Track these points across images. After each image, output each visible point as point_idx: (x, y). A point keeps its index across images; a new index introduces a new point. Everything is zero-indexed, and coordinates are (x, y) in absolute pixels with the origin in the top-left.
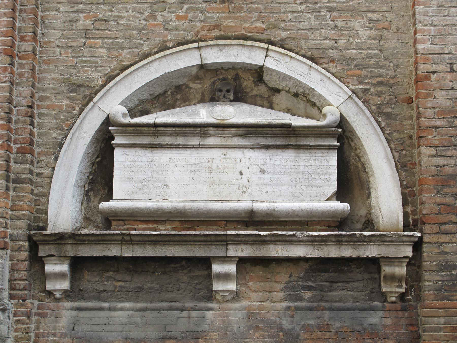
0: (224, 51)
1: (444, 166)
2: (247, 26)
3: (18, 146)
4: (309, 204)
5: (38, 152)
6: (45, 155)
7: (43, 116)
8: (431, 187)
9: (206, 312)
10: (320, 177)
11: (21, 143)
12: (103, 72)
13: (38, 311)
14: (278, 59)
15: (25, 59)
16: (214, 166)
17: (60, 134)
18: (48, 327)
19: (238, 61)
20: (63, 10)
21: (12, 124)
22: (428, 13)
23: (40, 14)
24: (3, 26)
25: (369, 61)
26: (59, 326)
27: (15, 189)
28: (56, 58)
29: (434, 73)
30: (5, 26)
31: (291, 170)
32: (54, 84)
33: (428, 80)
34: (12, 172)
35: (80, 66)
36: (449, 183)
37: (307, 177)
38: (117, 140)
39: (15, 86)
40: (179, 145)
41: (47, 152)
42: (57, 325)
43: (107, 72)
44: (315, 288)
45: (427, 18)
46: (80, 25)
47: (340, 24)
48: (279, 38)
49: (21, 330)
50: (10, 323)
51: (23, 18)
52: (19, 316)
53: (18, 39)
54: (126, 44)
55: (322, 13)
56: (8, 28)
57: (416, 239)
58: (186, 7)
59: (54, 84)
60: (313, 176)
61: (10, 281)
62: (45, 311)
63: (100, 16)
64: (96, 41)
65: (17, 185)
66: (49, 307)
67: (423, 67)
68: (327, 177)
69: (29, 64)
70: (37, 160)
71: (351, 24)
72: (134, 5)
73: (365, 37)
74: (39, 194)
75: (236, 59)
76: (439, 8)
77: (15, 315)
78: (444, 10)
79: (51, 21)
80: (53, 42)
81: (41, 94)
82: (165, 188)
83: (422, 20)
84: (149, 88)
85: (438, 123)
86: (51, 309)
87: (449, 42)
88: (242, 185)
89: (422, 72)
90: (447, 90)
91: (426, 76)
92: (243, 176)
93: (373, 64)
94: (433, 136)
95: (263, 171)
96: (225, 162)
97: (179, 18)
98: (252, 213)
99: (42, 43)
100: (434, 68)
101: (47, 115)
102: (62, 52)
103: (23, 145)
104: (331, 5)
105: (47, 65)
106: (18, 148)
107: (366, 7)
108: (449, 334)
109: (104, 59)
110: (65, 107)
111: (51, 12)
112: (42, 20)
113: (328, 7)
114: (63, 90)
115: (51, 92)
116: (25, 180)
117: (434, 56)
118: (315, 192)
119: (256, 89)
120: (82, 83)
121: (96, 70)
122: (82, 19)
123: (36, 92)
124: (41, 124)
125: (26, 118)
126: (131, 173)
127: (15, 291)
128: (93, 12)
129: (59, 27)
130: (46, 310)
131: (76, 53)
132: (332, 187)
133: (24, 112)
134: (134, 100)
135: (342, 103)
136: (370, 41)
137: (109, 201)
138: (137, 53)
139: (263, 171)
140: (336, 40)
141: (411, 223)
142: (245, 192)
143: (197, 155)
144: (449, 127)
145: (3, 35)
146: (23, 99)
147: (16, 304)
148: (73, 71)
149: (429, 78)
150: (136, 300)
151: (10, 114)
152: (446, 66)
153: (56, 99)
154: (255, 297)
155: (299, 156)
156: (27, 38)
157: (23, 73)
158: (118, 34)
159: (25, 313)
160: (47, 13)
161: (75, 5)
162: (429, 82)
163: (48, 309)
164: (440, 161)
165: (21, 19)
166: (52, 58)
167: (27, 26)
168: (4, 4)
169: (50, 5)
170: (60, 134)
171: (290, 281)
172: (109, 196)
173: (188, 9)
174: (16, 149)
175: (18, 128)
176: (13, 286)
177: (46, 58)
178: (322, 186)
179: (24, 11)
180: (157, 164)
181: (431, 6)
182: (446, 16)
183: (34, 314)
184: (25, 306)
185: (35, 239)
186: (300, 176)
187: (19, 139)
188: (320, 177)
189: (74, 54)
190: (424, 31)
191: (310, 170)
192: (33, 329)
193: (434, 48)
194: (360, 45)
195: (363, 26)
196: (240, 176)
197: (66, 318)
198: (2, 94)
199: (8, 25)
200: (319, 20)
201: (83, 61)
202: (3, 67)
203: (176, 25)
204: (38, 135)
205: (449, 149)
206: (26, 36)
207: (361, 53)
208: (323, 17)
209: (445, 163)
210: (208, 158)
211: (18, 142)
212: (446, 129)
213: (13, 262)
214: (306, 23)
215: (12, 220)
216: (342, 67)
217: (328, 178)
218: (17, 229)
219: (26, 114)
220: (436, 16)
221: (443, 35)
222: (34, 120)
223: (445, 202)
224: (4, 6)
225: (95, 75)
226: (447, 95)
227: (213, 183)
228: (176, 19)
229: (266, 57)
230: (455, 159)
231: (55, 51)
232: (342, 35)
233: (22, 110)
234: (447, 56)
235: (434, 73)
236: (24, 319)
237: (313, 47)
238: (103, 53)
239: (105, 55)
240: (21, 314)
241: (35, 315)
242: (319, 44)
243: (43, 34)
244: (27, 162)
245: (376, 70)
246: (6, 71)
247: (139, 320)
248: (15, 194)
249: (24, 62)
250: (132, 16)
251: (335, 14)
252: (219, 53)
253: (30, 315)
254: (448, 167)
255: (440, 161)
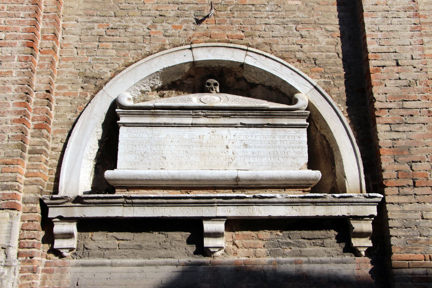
0: (212, 51)
1: (398, 139)
2: (229, 34)
3: (36, 123)
4: (287, 171)
5: (54, 130)
6: (60, 133)
7: (60, 102)
8: (389, 157)
9: (198, 267)
10: (294, 150)
11: (38, 121)
12: (112, 68)
13: (45, 268)
14: (256, 58)
15: (46, 53)
16: (205, 141)
17: (74, 116)
18: (53, 282)
19: (223, 59)
20: (81, 20)
21: (31, 104)
22: (374, 22)
23: (61, 23)
24: (26, 24)
25: (328, 61)
26: (64, 282)
27: (31, 159)
28: (73, 56)
29: (383, 67)
30: (28, 24)
31: (269, 145)
32: (71, 76)
33: (379, 72)
34: (28, 144)
35: (94, 63)
36: (403, 153)
37: (283, 150)
38: (123, 120)
39: (35, 75)
40: (175, 124)
41: (62, 130)
42: (62, 280)
43: (115, 68)
44: (293, 244)
45: (375, 26)
46: (94, 32)
47: (304, 33)
48: (255, 43)
49: (25, 285)
50: (16, 279)
51: (46, 22)
52: (26, 272)
53: (40, 38)
54: (132, 46)
55: (289, 25)
56: (31, 26)
57: (380, 200)
58: (181, 19)
59: (71, 76)
60: (288, 149)
61: (20, 239)
62: (52, 268)
63: (111, 25)
64: (107, 44)
65: (32, 155)
66: (55, 264)
67: (374, 62)
68: (300, 150)
69: (49, 58)
70: (53, 137)
71: (312, 34)
72: (139, 17)
73: (324, 43)
74: (52, 165)
75: (222, 58)
76: (383, 19)
77: (21, 271)
78: (387, 20)
79: (70, 28)
80: (71, 44)
81: (59, 84)
82: (163, 160)
83: (370, 27)
84: (150, 81)
85: (390, 105)
86: (57, 266)
87: (393, 43)
88: (228, 157)
89: (374, 66)
90: (395, 79)
91: (376, 69)
92: (229, 150)
93: (332, 63)
94: (386, 115)
95: (246, 146)
96: (213, 138)
97: (175, 28)
98: (237, 179)
99: (62, 45)
100: (383, 63)
101: (64, 101)
102: (78, 52)
103: (40, 122)
104: (296, 19)
105: (65, 62)
106: (35, 125)
107: (324, 21)
108: (418, 284)
109: (113, 57)
110: (79, 94)
111: (71, 22)
112: (63, 28)
113: (295, 21)
114: (78, 81)
115: (67, 83)
116: (40, 151)
117: (382, 54)
118: (290, 162)
119: (237, 84)
120: (95, 76)
121: (106, 66)
122: (96, 28)
123: (55, 83)
124: (58, 108)
125: (44, 100)
126: (133, 147)
127: (24, 249)
128: (106, 22)
129: (77, 33)
130: (53, 267)
131: (90, 52)
132: (305, 158)
133: (43, 96)
134: (137, 90)
135: (309, 92)
136: (328, 46)
137: (114, 170)
138: (140, 54)
139: (246, 146)
140: (301, 45)
141: (372, 188)
142: (231, 163)
143: (190, 133)
144: (399, 109)
145: (27, 31)
146: (42, 85)
147: (23, 261)
148: (87, 67)
149: (379, 70)
150: (135, 256)
151: (29, 94)
152: (393, 62)
153: (72, 88)
154: (241, 253)
155: (275, 134)
156: (48, 38)
157: (44, 64)
158: (126, 39)
159: (31, 269)
160: (68, 22)
161: (91, 17)
162: (379, 73)
163: (55, 266)
164: (395, 135)
165: (44, 23)
166: (70, 56)
167: (49, 29)
168: (29, 7)
169: (71, 16)
170: (74, 116)
171: (271, 238)
172: (114, 167)
173: (182, 21)
174: (33, 126)
175: (37, 108)
176: (22, 244)
177: (65, 56)
178: (296, 158)
179: (47, 17)
180: (155, 140)
181: (377, 17)
182: (389, 24)
183: (41, 271)
184: (32, 262)
185: (45, 201)
186: (277, 149)
187: (36, 117)
188: (294, 150)
189: (88, 53)
190: (373, 35)
191: (285, 145)
192: (39, 284)
193: (382, 48)
194: (320, 48)
195: (322, 35)
196: (226, 150)
197: (71, 273)
198: (23, 78)
199: (31, 23)
200: (287, 30)
201: (95, 59)
202: (25, 57)
203: (173, 33)
204: (55, 117)
205: (401, 126)
206: (47, 36)
207: (322, 55)
208: (289, 28)
209: (398, 137)
210: (199, 135)
211: (36, 120)
212: (397, 110)
213: (23, 222)
214: (276, 33)
215: (26, 185)
216: (307, 65)
217: (300, 151)
218: (29, 193)
219: (44, 97)
220: (381, 24)
221: (388, 38)
222: (51, 103)
223: (401, 168)
224: (28, 9)
225: (105, 70)
226: (395, 84)
227: (204, 155)
228: (173, 28)
229: (246, 56)
230: (406, 134)
231: (72, 51)
232: (306, 41)
233: (41, 94)
234: (392, 54)
235: (383, 67)
236: (29, 275)
237: (283, 50)
238: (112, 53)
239: (114, 54)
240: (27, 271)
241: (42, 272)
242: (288, 48)
243: (63, 38)
244: (43, 136)
245: (334, 68)
246: (27, 59)
247: (138, 275)
248: (30, 163)
249: (45, 56)
250: (137, 26)
251: (300, 26)
252: (208, 53)
253: (37, 271)
254: (401, 140)
255: (395, 135)
